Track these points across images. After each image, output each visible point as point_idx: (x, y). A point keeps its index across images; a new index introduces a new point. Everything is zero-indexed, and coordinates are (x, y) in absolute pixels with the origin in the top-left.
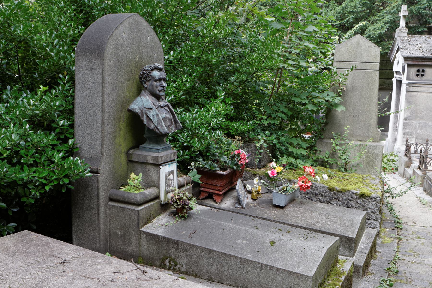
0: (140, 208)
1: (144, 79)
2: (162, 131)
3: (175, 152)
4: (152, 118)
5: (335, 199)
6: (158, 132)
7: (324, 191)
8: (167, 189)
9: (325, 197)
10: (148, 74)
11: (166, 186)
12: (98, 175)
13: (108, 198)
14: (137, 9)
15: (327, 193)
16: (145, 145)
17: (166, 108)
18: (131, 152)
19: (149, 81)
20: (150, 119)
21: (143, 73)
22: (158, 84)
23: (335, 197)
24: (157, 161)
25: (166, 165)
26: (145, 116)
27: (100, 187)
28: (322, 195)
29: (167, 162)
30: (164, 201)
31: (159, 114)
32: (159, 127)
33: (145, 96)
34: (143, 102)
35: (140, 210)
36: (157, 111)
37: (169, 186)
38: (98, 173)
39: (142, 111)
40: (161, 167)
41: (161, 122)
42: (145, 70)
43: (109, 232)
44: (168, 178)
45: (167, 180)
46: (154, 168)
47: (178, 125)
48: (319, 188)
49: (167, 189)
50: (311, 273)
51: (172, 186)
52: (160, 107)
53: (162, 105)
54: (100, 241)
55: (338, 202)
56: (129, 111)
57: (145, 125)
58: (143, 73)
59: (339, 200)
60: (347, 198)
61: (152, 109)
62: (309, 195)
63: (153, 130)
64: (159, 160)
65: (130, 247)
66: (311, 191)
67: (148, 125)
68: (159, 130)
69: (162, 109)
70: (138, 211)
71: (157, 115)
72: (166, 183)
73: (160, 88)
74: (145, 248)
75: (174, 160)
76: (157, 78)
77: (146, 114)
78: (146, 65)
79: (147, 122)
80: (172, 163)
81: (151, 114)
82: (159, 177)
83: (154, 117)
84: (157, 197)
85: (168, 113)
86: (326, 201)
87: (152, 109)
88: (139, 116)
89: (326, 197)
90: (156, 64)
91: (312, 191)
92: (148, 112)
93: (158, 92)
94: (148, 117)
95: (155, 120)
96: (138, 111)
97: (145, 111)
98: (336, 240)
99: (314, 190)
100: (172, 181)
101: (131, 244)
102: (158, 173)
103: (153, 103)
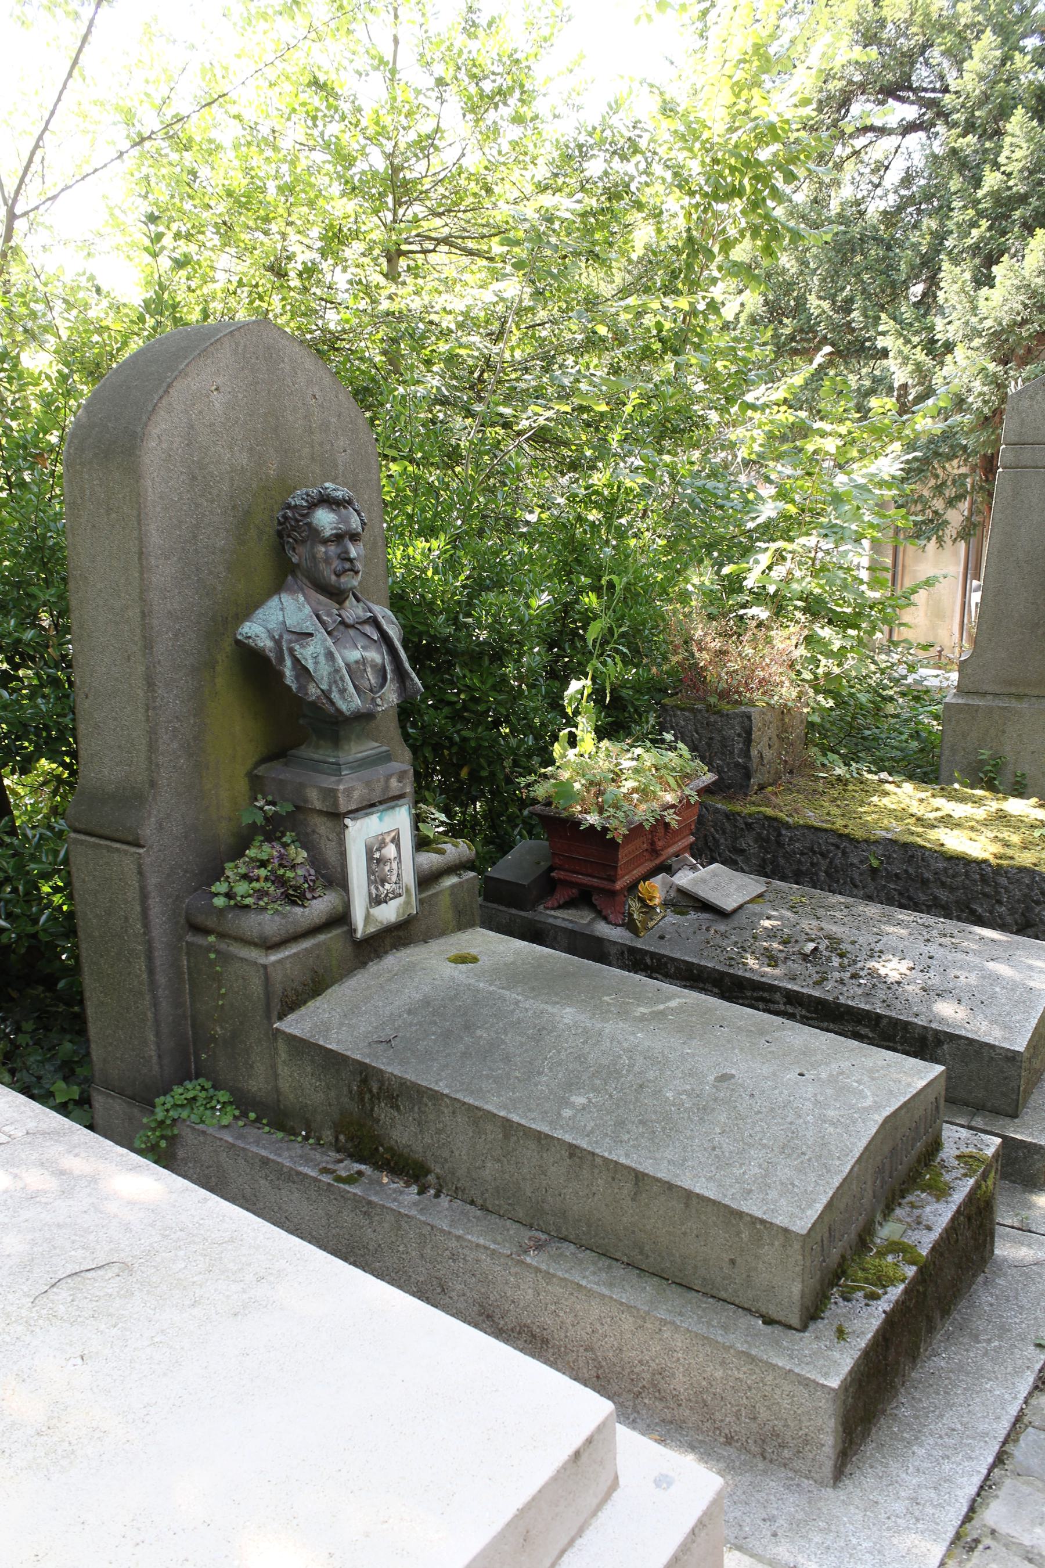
0: (273, 958)
1: (289, 536)
2: (343, 706)
3: (405, 772)
4: (310, 666)
5: (985, 895)
6: (332, 710)
7: (951, 872)
8: (374, 891)
9: (952, 889)
10: (298, 521)
11: (370, 882)
12: (141, 851)
13: (182, 921)
14: (356, 296)
15: (959, 879)
16: (306, 752)
17: (369, 630)
18: (261, 771)
19: (303, 542)
20: (306, 669)
21: (285, 517)
22: (332, 549)
23: (987, 890)
24: (336, 803)
25: (372, 813)
26: (288, 662)
27: (150, 888)
28: (943, 885)
29: (373, 805)
30: (364, 931)
31: (333, 649)
32: (335, 696)
33: (295, 592)
34: (281, 616)
35: (273, 964)
36: (329, 642)
37: (383, 881)
38: (143, 847)
39: (278, 642)
40: (347, 821)
41: (342, 679)
42: (289, 506)
43: (193, 1026)
44: (377, 855)
45: (375, 861)
46: (329, 824)
47: (408, 683)
48: (932, 861)
49: (374, 891)
50: (802, 1224)
51: (394, 878)
52: (342, 628)
53: (350, 621)
54: (159, 1056)
55: (997, 907)
56: (238, 642)
57: (289, 688)
58: (285, 517)
59: (999, 902)
60: (1025, 895)
61: (311, 635)
62: (901, 883)
63: (313, 704)
64: (342, 800)
65: (250, 1076)
66: (906, 871)
67: (299, 688)
68: (333, 703)
69: (352, 632)
70: (265, 967)
71: (330, 656)
72: (370, 872)
73: (336, 564)
74: (300, 1086)
75: (401, 796)
76: (328, 533)
77: (291, 651)
78: (295, 489)
79: (297, 677)
80: (393, 808)
81: (310, 653)
82: (343, 854)
83: (316, 663)
84: (341, 918)
85: (374, 646)
86: (957, 902)
87: (311, 635)
88: (267, 659)
89: (957, 888)
90: (327, 485)
91: (910, 870)
92: (297, 647)
93: (333, 578)
94: (296, 661)
95: (322, 671)
96: (265, 643)
97: (290, 641)
98: (931, 1076)
99: (919, 867)
100: (395, 865)
101: (252, 1067)
102: (341, 843)
103: (318, 617)
